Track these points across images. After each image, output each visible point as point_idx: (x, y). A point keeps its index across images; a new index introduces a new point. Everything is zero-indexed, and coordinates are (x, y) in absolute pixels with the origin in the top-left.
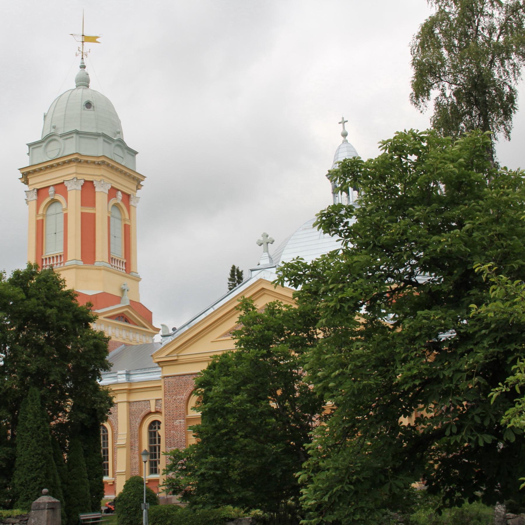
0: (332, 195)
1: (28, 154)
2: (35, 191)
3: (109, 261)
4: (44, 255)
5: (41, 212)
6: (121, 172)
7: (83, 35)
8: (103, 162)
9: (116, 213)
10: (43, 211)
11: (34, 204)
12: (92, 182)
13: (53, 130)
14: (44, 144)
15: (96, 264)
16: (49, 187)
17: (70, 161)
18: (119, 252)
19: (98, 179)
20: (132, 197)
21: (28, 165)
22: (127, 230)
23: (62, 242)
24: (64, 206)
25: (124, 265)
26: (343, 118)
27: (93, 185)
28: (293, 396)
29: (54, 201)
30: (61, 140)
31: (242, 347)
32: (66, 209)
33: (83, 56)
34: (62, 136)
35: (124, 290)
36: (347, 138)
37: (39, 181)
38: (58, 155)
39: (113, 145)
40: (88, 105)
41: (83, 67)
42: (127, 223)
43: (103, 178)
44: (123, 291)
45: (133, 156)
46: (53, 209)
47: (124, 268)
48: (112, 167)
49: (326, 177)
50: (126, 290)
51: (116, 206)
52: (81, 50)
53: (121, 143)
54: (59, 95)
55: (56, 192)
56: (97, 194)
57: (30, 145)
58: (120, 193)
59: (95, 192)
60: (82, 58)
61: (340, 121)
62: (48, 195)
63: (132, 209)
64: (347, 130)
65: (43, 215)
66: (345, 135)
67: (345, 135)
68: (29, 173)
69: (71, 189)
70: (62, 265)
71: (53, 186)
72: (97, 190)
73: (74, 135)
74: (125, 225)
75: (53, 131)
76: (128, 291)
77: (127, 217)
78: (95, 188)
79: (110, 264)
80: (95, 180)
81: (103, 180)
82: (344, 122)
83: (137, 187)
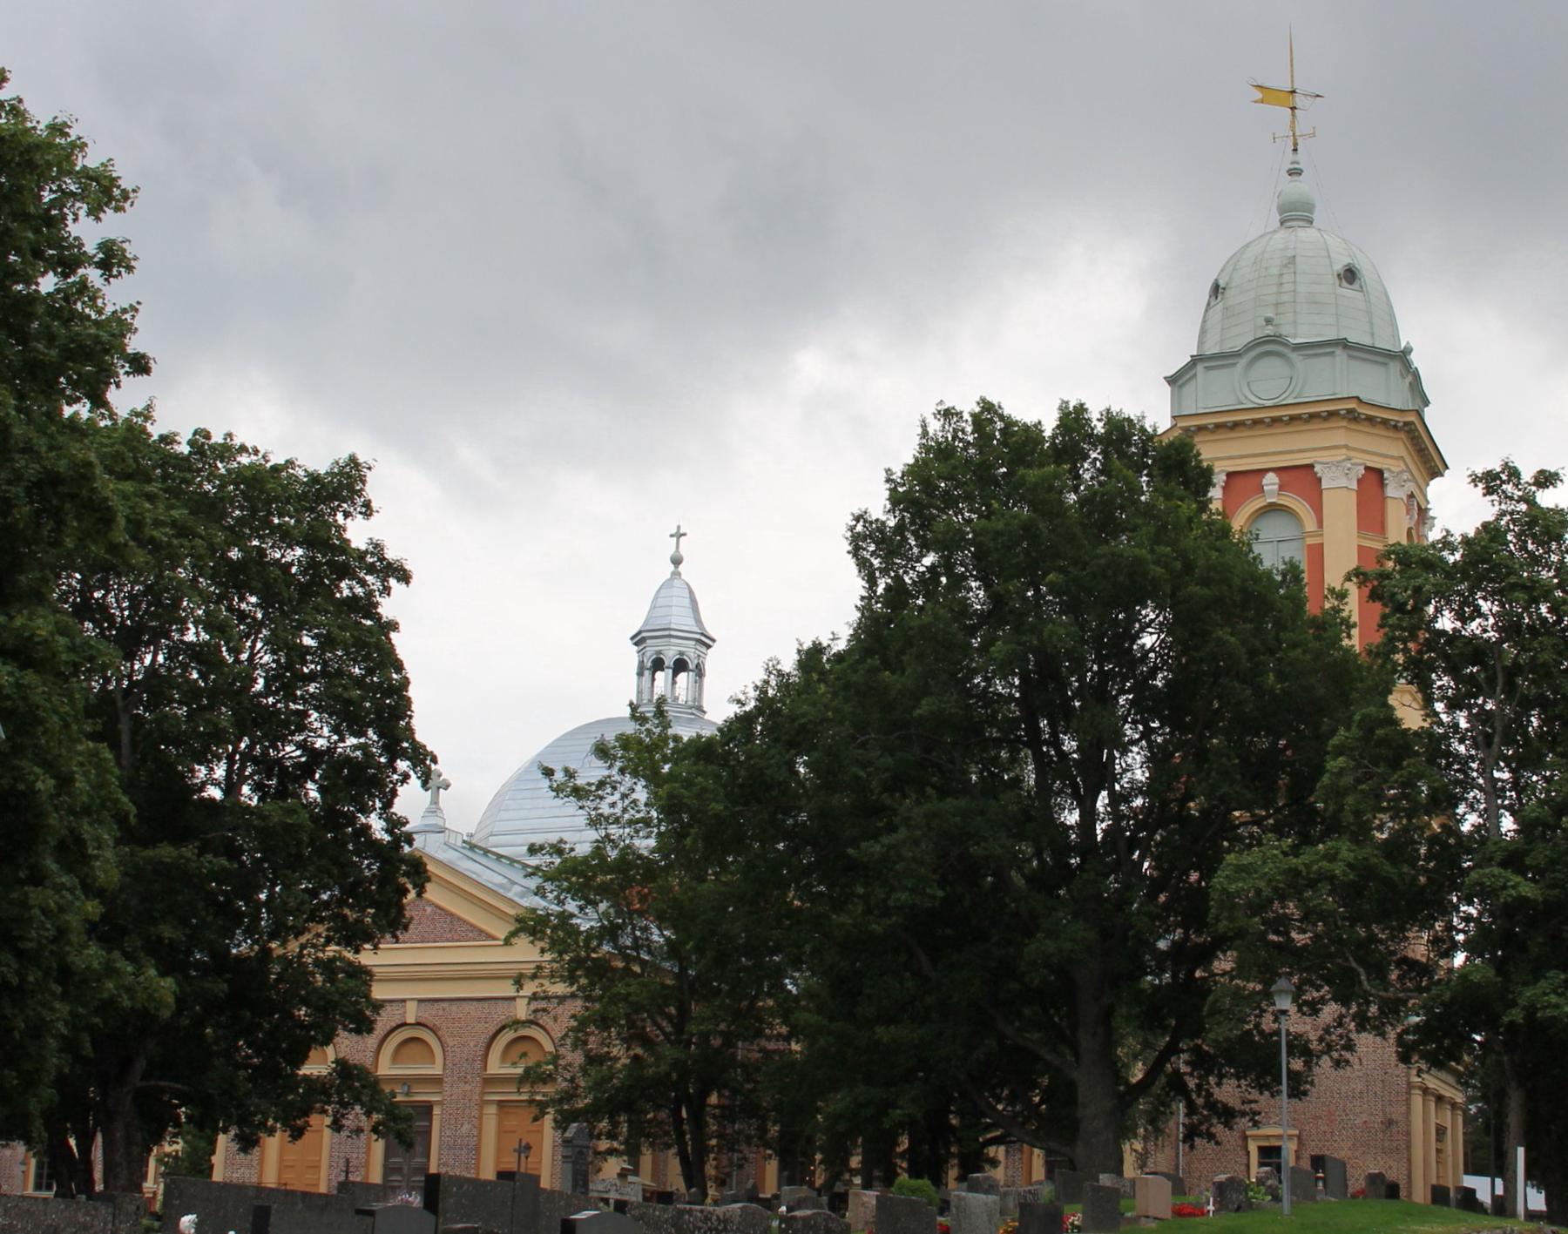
0: (636, 677)
14: (1243, 362)
16: (1263, 472)
24: (1310, 525)
26: (679, 527)
28: (952, 1112)
30: (1294, 356)
31: (583, 981)
36: (681, 568)
40: (1350, 275)
49: (630, 642)
54: (1245, 243)
56: (1389, 502)
59: (1384, 498)
60: (1295, 150)
61: (674, 531)
62: (1260, 489)
64: (683, 551)
66: (677, 561)
67: (677, 561)
71: (1277, 470)
73: (1338, 351)
75: (1269, 330)
80: (1389, 470)
82: (679, 535)
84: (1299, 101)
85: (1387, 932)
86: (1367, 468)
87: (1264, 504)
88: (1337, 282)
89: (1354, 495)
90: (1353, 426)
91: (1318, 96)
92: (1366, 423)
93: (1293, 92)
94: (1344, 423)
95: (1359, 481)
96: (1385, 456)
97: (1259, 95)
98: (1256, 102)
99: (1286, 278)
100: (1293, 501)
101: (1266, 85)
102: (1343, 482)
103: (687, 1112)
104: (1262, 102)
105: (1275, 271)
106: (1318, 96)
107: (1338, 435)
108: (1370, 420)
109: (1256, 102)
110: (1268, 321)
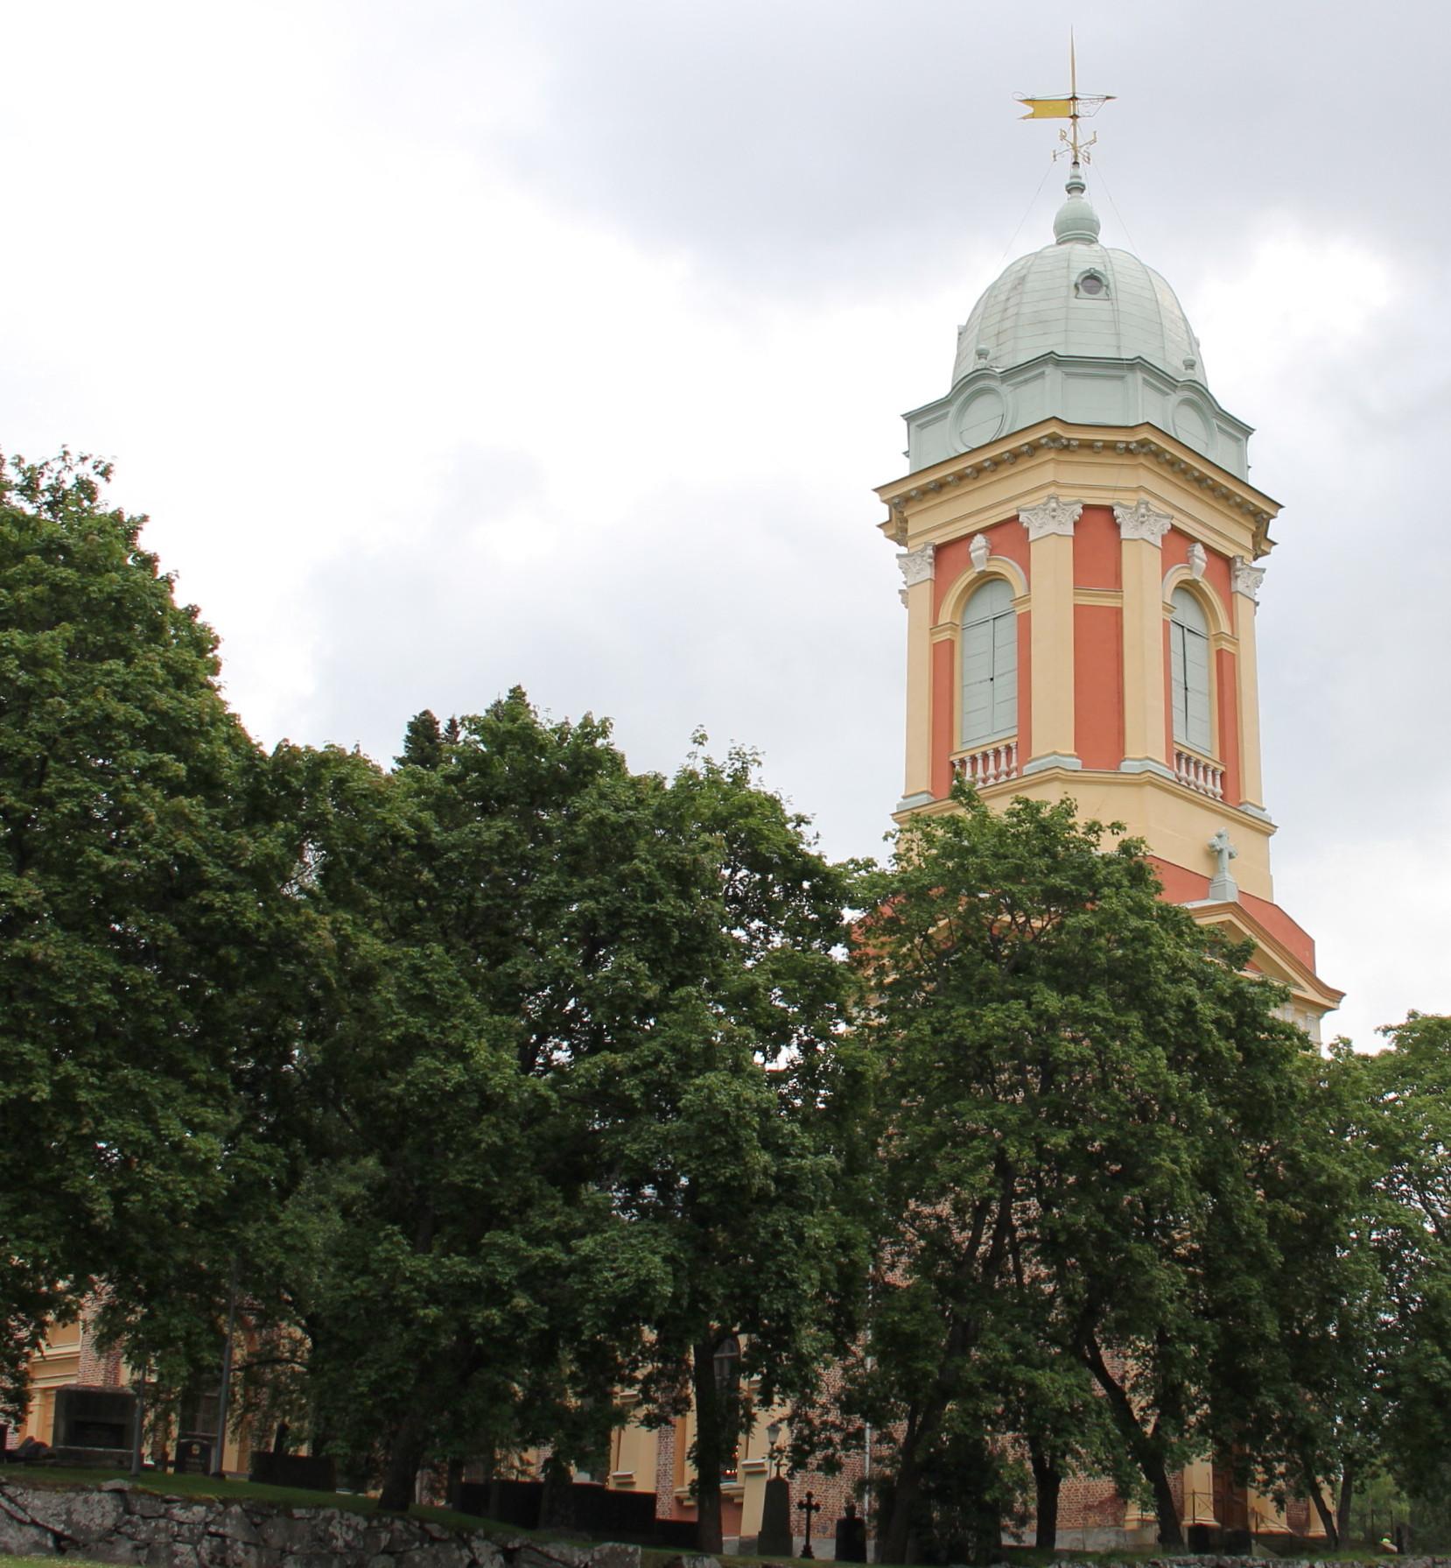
1: (906, 454)
2: (930, 552)
3: (1169, 759)
4: (957, 748)
5: (945, 617)
6: (1201, 481)
7: (1075, 117)
8: (1143, 444)
9: (1188, 613)
10: (954, 613)
11: (926, 592)
12: (1110, 509)
13: (983, 360)
14: (953, 409)
15: (1126, 766)
16: (970, 537)
17: (1035, 448)
18: (1200, 738)
19: (1130, 499)
20: (1239, 565)
21: (907, 473)
22: (1226, 670)
23: (1014, 676)
25: (1218, 782)
27: (1115, 519)
29: (988, 580)
30: (1004, 389)
32: (1026, 599)
33: (1076, 156)
34: (1010, 374)
35: (1220, 851)
37: (940, 522)
38: (1000, 429)
39: (1175, 398)
40: (1092, 281)
41: (1076, 188)
42: (1226, 646)
43: (1144, 496)
44: (1214, 854)
45: (1239, 440)
46: (990, 603)
47: (1219, 790)
48: (1173, 463)
50: (1226, 855)
51: (1188, 588)
52: (1070, 138)
53: (1199, 398)
55: (993, 551)
57: (910, 418)
58: (1199, 550)
60: (1076, 163)
62: (969, 562)
63: (1242, 604)
65: (953, 626)
68: (907, 499)
69: (1042, 533)
70: (1014, 775)
71: (983, 531)
72: (1125, 533)
73: (1049, 370)
74: (1220, 652)
75: (982, 363)
76: (1231, 856)
77: (1225, 628)
78: (1118, 527)
79: (1171, 768)
80: (1121, 505)
81: (1147, 503)
83: (1256, 544)
84: (1080, 108)
85: (606, 1156)
86: (1086, 507)
87: (974, 575)
88: (1073, 292)
89: (1158, 554)
90: (1063, 458)
91: (1108, 98)
92: (1106, 452)
93: (1074, 98)
94: (1052, 455)
95: (1163, 537)
96: (1115, 489)
97: (1029, 110)
98: (1024, 118)
99: (1012, 301)
100: (1006, 566)
101: (1038, 96)
102: (1052, 527)
103: (344, 1496)
104: (1033, 116)
105: (1003, 297)
106: (1108, 98)
107: (1046, 471)
108: (1088, 446)
109: (1024, 118)
110: (981, 354)
